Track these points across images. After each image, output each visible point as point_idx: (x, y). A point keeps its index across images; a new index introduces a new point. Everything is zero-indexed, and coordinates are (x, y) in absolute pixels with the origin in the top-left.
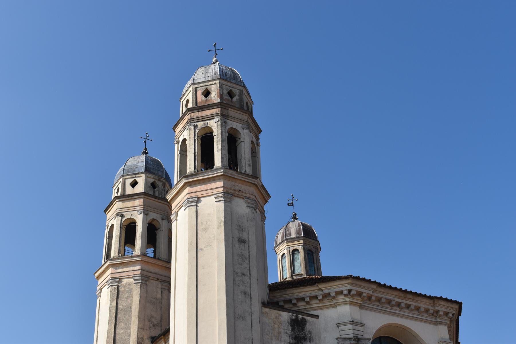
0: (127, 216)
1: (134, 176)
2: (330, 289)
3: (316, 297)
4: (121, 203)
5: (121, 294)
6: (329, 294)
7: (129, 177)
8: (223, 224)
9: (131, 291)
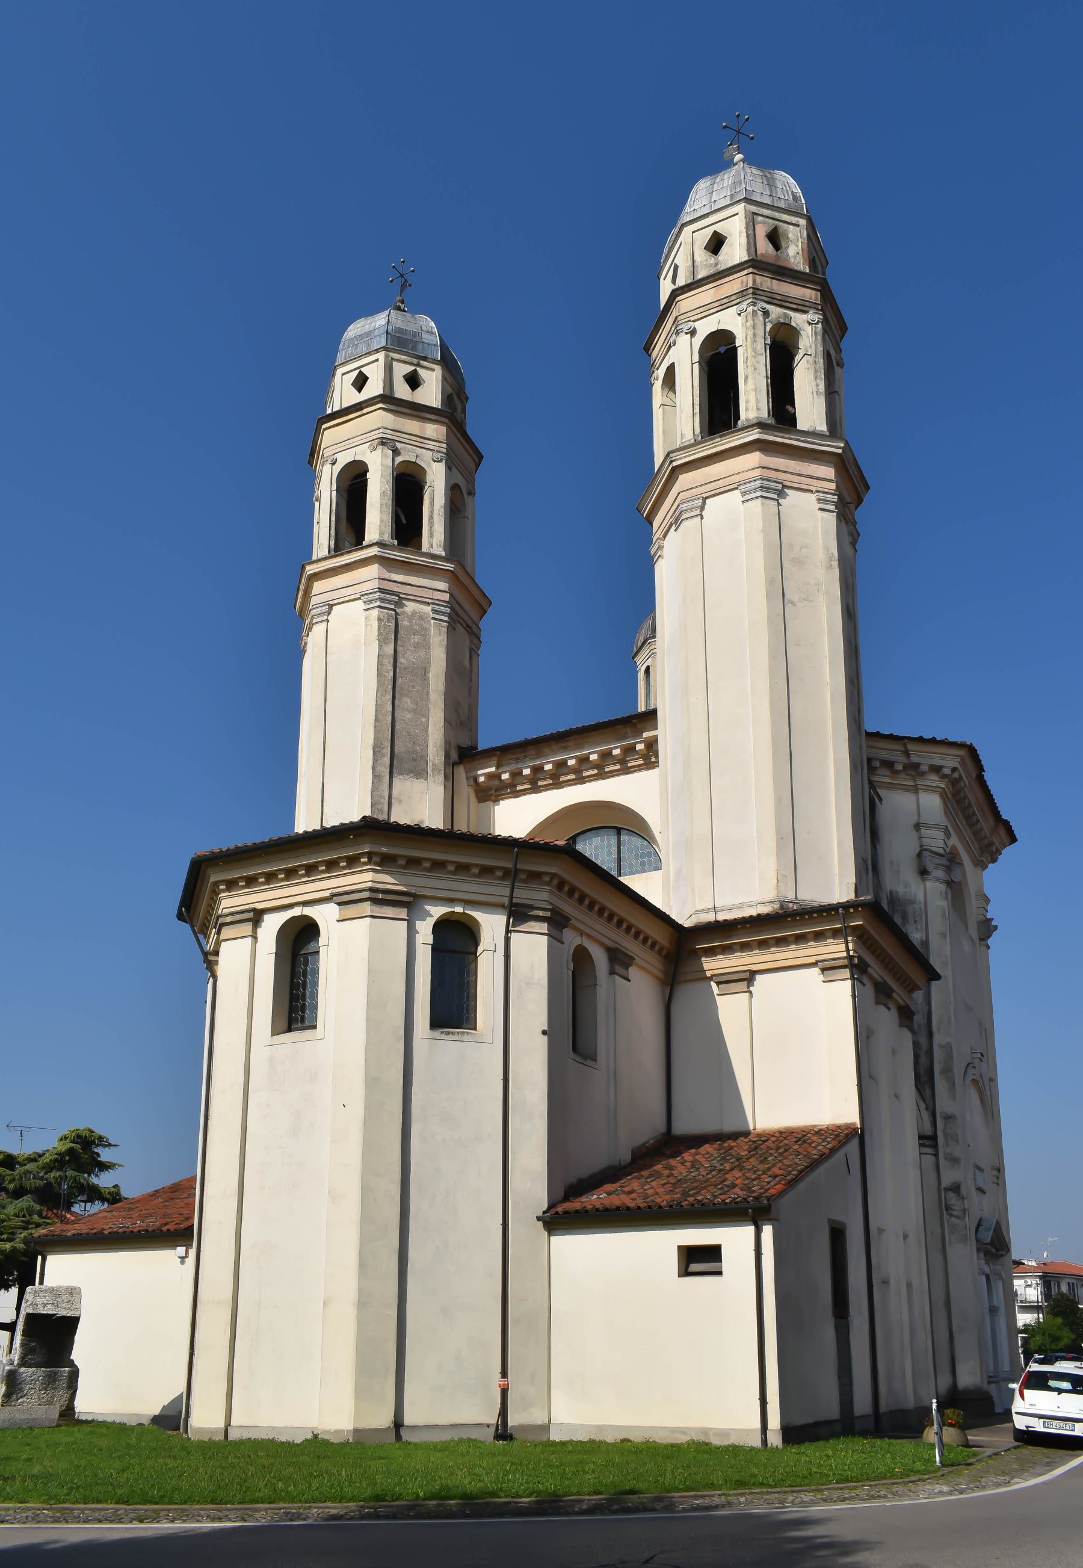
0: (408, 455)
1: (415, 361)
2: (923, 756)
3: (889, 764)
4: (390, 417)
5: (401, 632)
6: (916, 766)
7: (403, 357)
8: (835, 564)
9: (424, 632)
